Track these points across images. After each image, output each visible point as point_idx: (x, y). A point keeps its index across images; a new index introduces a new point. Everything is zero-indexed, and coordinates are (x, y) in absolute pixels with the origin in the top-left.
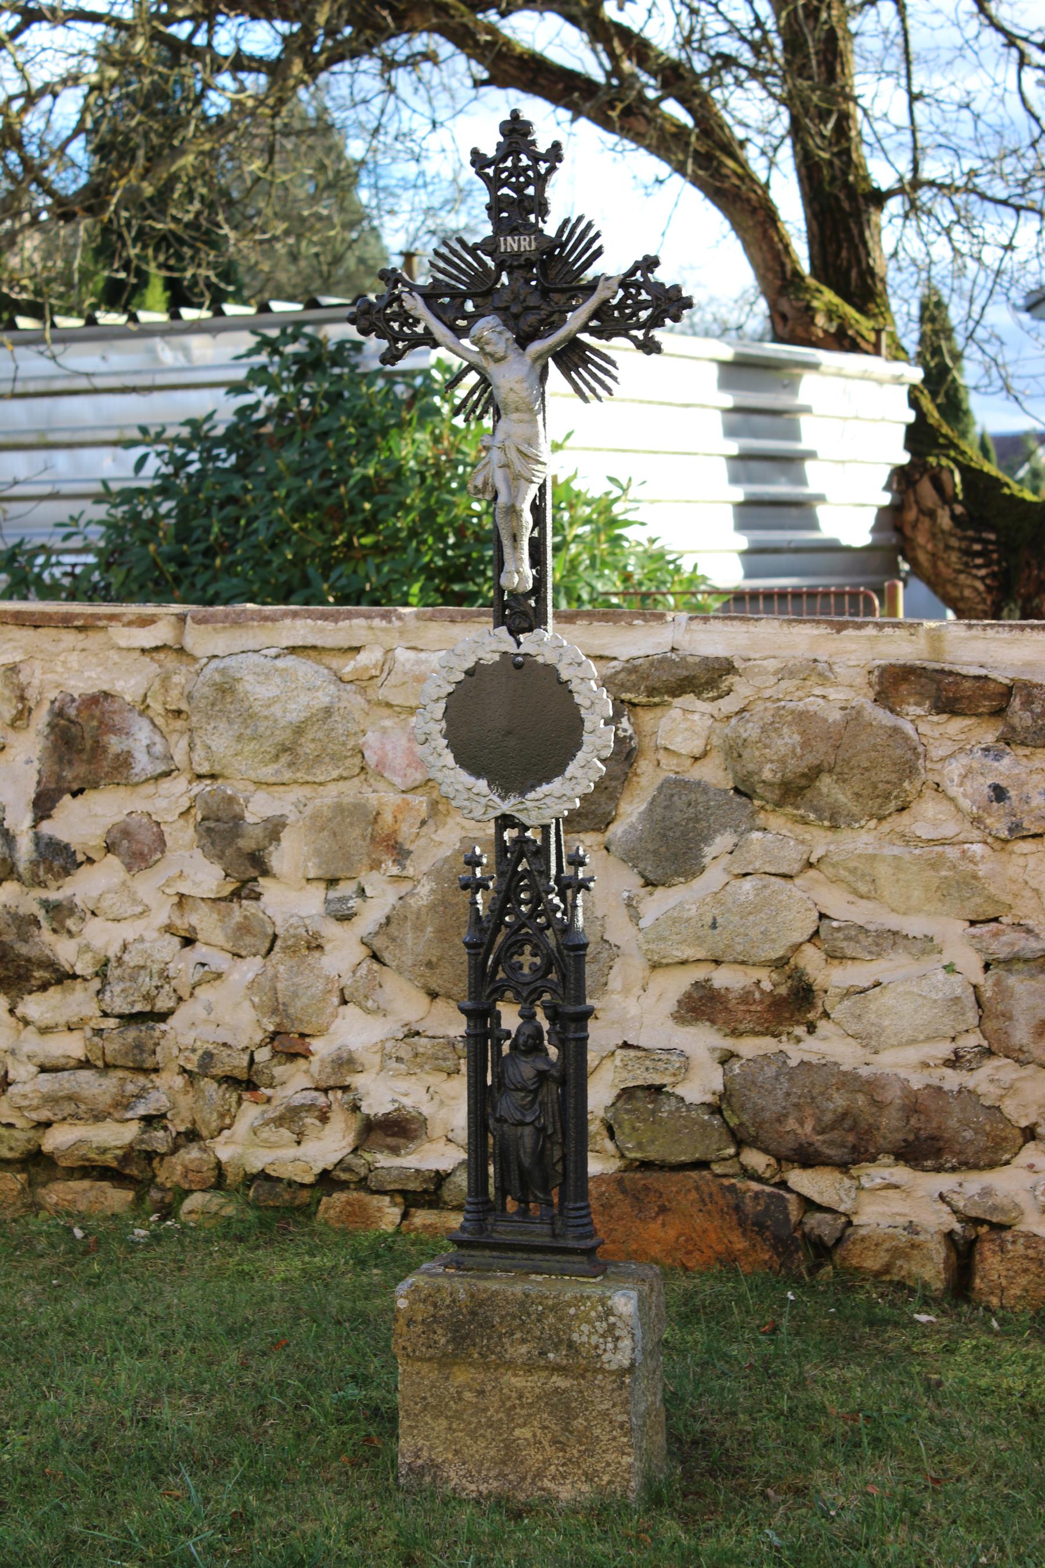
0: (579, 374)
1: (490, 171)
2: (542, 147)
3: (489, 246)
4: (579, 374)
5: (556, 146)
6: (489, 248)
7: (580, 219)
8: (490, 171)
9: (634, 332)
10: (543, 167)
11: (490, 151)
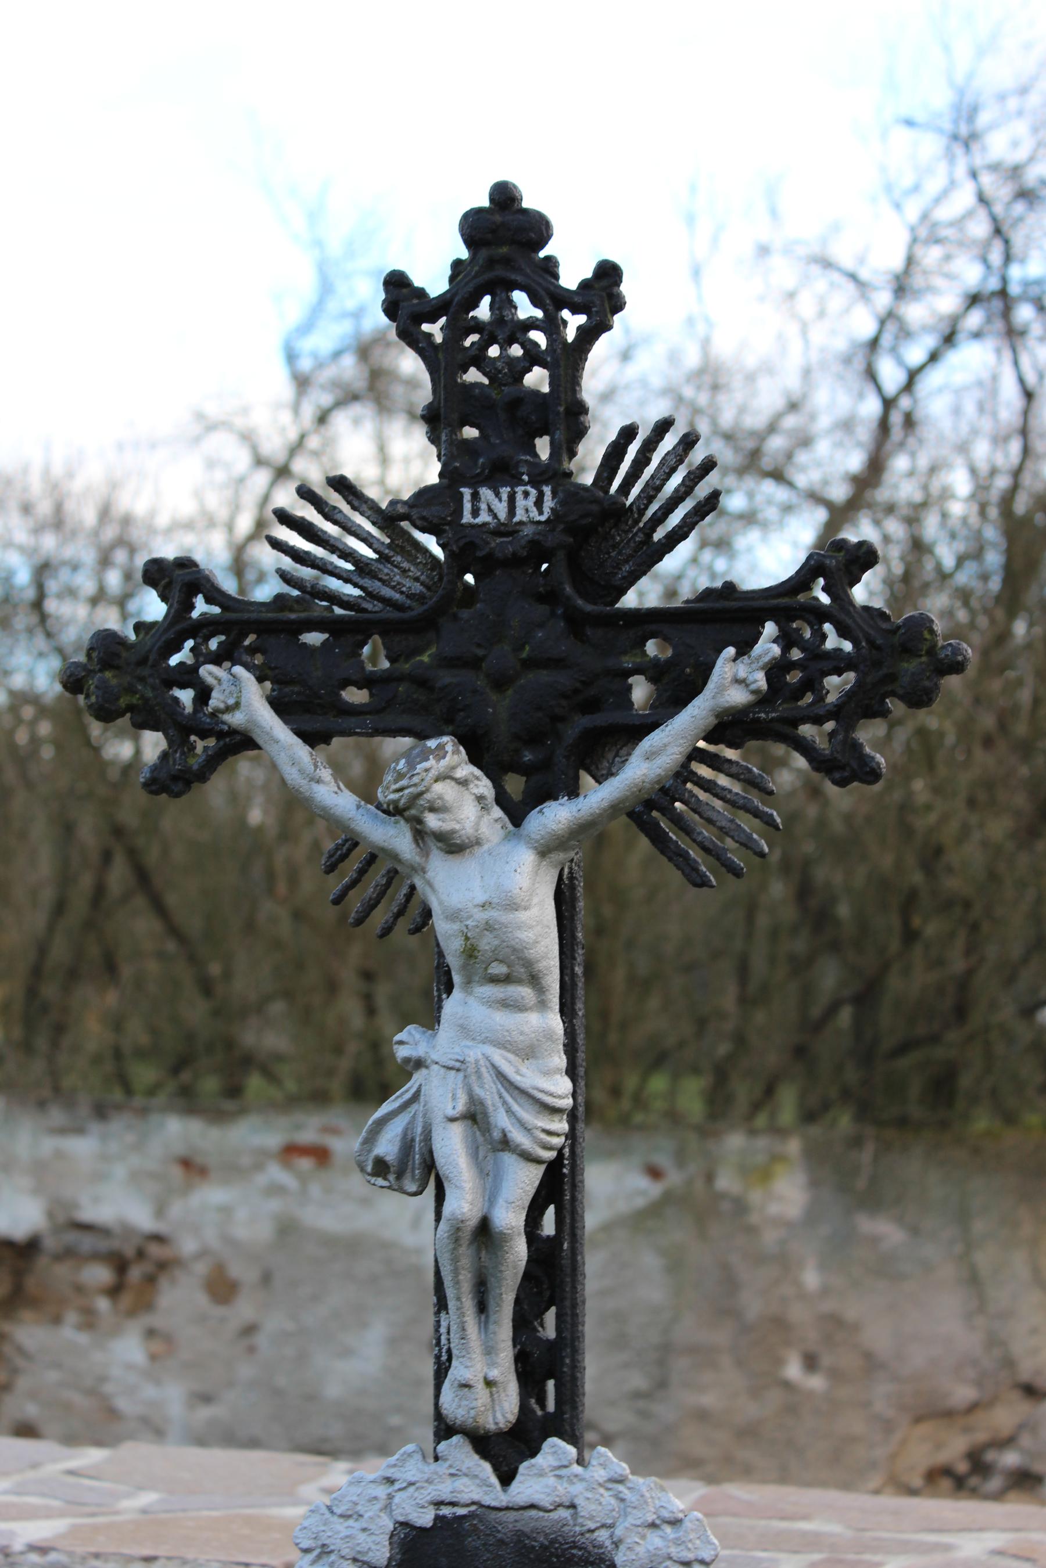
0: (626, 487)
1: (435, 330)
2: (572, 275)
3: (431, 507)
4: (626, 487)
5: (608, 275)
6: (433, 512)
7: (663, 427)
8: (435, 330)
9: (807, 730)
10: (573, 322)
11: (433, 280)
